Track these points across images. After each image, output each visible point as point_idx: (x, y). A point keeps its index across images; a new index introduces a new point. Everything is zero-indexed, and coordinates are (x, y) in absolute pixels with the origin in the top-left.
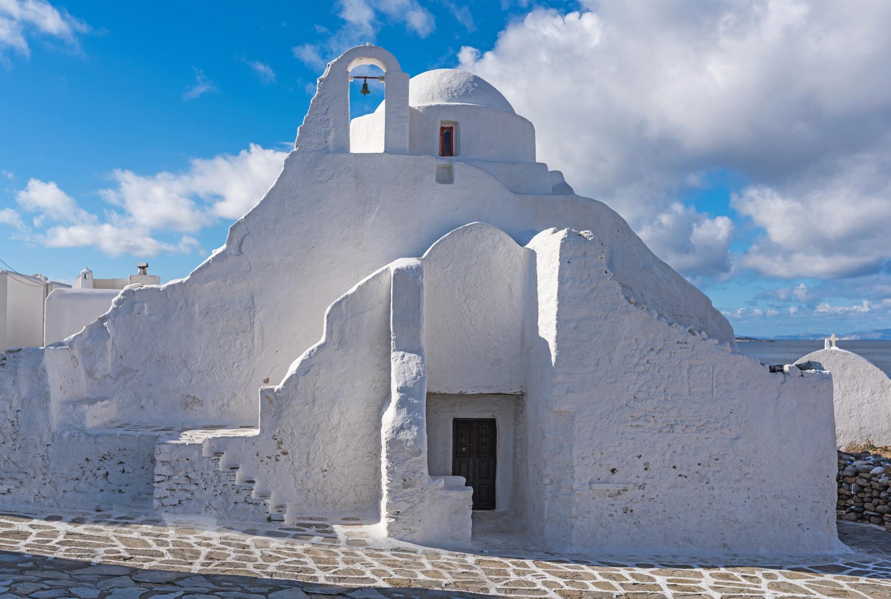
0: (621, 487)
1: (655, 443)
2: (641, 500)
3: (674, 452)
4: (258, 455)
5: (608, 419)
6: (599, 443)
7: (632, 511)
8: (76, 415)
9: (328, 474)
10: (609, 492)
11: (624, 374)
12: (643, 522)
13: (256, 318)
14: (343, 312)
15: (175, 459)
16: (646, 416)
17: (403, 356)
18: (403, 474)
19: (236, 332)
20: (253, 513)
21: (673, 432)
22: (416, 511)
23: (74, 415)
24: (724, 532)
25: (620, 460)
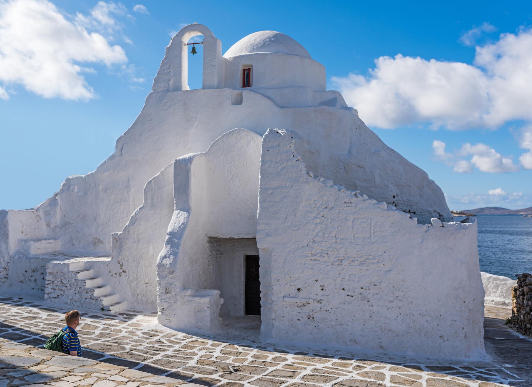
0: (304, 301)
1: (328, 271)
2: (320, 311)
3: (343, 279)
4: (110, 272)
5: (294, 254)
6: (288, 270)
7: (314, 318)
8: (26, 247)
9: (149, 285)
10: (297, 304)
11: (305, 224)
12: (321, 326)
13: (131, 192)
14: (153, 187)
15: (56, 272)
16: (321, 253)
17: (179, 213)
20: (94, 305)
21: (342, 264)
22: (172, 308)
23: (25, 247)
24: (381, 337)
25: (303, 282)
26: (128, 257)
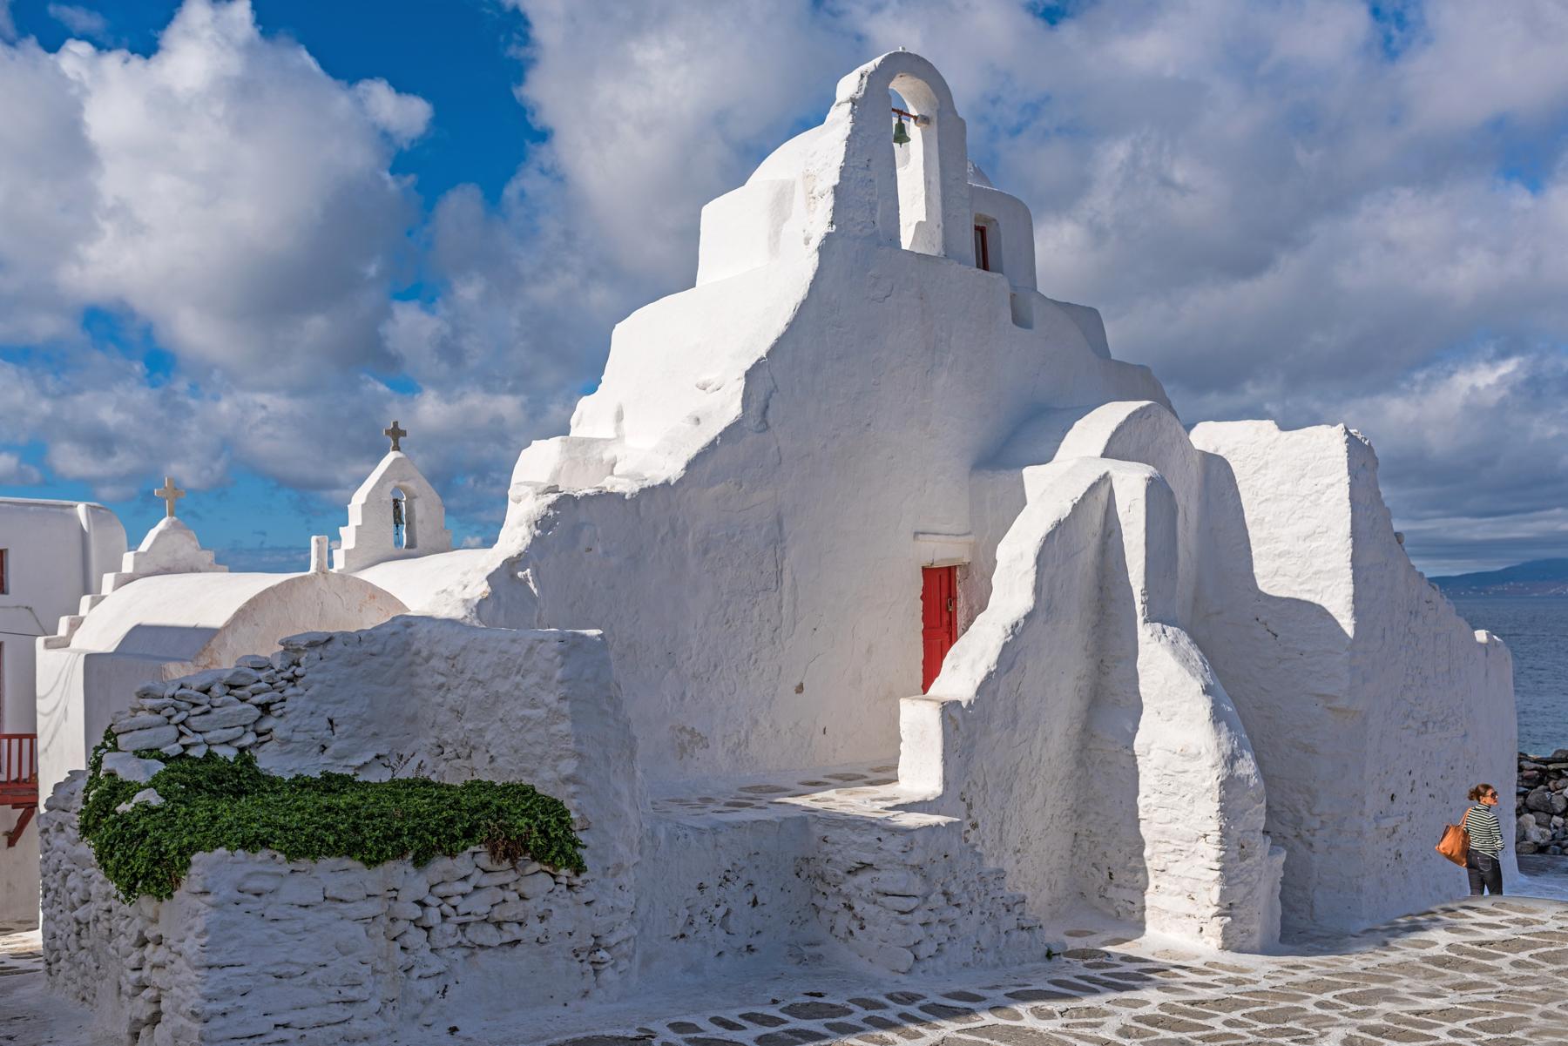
13: (786, 562)
18: (1240, 835)
19: (752, 591)
26: (985, 775)
